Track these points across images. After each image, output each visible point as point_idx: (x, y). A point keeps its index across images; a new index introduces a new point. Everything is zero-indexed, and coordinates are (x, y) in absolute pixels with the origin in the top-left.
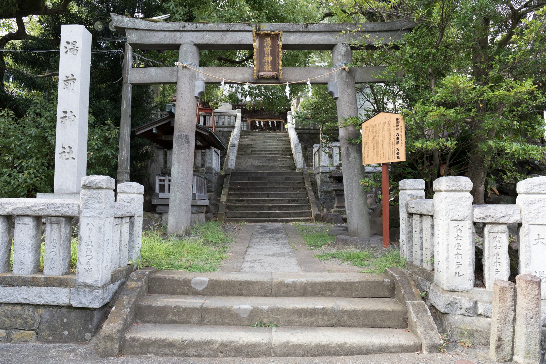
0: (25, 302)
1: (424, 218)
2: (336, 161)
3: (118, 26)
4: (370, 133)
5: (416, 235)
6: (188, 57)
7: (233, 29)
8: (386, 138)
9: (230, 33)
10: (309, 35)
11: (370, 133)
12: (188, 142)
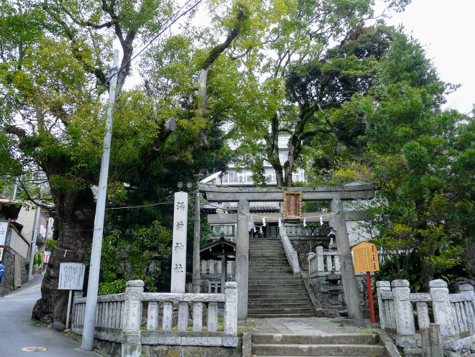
0: (200, 345)
1: (390, 301)
2: (330, 267)
5: (387, 311)
10: (316, 194)
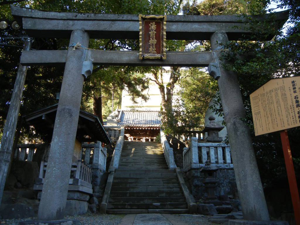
2: (205, 159)
3: (16, 14)
4: (260, 102)
6: (78, 40)
7: (121, 18)
8: (282, 103)
9: (119, 22)
10: (189, 24)
11: (260, 102)
12: (71, 116)
